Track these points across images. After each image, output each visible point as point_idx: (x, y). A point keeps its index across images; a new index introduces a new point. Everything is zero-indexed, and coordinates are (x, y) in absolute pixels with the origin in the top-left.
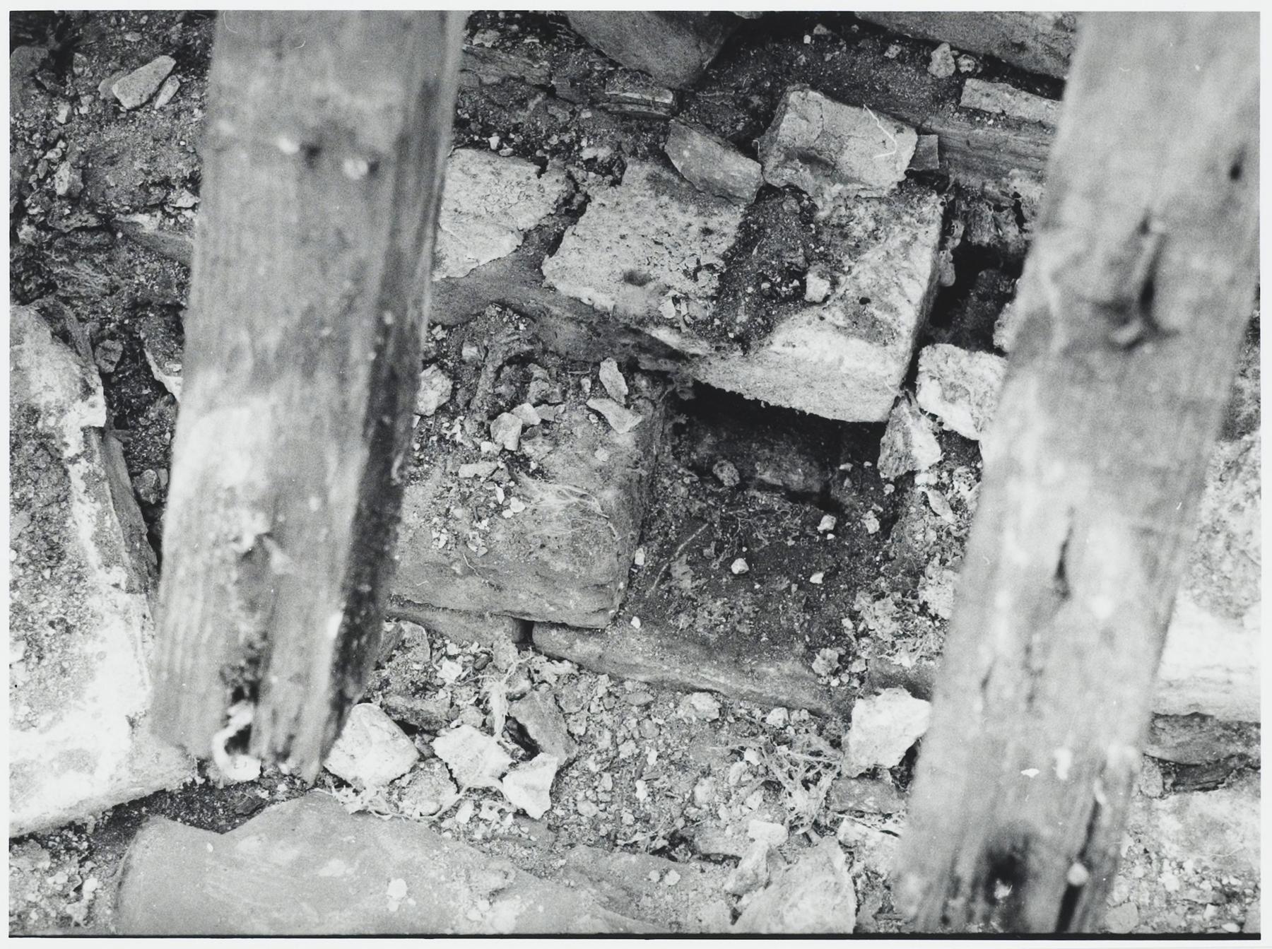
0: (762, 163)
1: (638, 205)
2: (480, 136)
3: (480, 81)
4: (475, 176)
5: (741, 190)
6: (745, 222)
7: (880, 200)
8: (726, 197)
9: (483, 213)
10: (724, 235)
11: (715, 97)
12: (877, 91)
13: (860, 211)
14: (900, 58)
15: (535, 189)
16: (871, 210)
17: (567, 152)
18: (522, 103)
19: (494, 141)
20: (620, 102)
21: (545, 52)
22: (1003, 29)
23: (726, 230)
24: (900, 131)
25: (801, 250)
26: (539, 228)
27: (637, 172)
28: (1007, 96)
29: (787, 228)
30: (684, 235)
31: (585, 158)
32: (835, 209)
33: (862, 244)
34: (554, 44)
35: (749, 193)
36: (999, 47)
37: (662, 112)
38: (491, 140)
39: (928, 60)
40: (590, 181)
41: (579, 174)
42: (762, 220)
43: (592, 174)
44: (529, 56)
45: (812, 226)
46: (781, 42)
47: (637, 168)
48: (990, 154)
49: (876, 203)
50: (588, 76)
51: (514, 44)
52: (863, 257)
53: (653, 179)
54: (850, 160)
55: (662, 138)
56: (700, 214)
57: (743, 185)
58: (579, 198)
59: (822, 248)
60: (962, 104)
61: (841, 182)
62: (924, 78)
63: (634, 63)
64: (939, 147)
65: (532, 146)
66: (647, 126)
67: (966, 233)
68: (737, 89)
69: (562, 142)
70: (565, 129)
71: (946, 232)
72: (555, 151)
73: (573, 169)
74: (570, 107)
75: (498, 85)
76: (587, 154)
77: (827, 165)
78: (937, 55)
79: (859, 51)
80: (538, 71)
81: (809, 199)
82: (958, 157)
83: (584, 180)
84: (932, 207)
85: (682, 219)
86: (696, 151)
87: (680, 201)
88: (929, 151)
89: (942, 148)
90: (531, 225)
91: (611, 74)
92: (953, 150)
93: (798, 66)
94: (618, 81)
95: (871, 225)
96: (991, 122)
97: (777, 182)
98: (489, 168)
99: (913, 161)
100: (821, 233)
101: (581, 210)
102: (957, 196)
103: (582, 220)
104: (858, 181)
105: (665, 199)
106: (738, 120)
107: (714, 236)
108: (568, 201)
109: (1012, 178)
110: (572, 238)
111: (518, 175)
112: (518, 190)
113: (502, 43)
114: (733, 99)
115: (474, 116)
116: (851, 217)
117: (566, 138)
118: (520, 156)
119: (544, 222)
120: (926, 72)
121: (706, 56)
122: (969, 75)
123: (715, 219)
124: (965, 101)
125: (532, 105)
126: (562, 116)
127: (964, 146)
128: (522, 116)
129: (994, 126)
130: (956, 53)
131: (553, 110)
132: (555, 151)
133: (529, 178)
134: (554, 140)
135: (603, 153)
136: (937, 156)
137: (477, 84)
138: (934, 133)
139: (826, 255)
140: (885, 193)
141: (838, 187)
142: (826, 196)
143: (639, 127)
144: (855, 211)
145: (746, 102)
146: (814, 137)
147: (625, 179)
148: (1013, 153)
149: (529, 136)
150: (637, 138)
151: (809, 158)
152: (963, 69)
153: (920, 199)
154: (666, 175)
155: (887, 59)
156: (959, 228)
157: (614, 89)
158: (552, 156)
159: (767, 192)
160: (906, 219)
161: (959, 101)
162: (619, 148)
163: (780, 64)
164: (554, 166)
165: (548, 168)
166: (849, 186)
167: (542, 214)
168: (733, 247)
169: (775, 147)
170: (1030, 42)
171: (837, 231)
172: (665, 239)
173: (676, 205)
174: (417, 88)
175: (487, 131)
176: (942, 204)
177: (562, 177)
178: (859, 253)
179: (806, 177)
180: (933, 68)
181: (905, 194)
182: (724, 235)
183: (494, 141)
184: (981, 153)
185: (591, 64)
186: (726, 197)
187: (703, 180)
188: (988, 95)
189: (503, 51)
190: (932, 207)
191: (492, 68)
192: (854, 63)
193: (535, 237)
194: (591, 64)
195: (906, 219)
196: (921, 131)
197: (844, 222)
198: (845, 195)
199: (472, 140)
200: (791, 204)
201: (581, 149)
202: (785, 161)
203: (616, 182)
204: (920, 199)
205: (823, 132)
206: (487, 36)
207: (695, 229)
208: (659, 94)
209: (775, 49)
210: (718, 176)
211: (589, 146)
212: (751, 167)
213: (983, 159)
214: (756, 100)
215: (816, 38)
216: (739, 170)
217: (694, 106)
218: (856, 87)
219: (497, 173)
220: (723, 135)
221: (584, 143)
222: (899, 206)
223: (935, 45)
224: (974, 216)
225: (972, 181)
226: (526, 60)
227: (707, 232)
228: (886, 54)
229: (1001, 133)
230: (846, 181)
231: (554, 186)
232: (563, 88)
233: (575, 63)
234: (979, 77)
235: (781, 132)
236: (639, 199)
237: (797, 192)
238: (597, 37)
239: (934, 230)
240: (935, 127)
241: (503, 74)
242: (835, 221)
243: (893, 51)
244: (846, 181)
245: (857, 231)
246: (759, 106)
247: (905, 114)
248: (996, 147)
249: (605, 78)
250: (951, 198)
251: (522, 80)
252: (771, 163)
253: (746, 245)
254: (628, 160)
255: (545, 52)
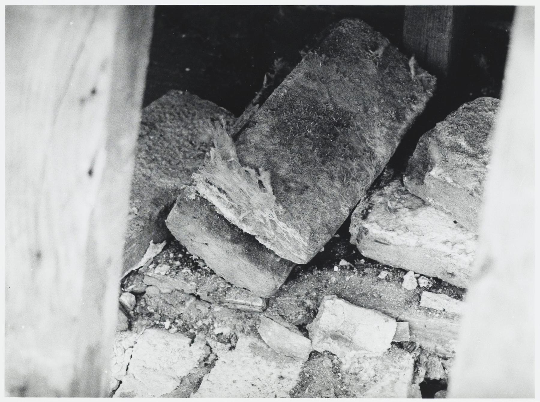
0: (311, 340)
1: (244, 362)
2: (160, 321)
3: (160, 291)
4: (155, 345)
5: (300, 354)
6: (303, 372)
7: (377, 358)
8: (292, 358)
9: (158, 368)
10: (291, 379)
11: (285, 300)
12: (374, 297)
13: (366, 365)
14: (387, 279)
15: (188, 353)
16: (373, 364)
17: (206, 329)
18: (182, 303)
19: (167, 324)
20: (234, 304)
21: (193, 277)
22: (442, 265)
23: (292, 377)
24: (387, 321)
25: (333, 389)
26: (190, 375)
27: (244, 342)
28: (446, 301)
29: (325, 377)
30: (268, 380)
31: (216, 333)
32: (352, 365)
33: (367, 385)
34: (199, 272)
35: (305, 356)
36: (440, 273)
37: (257, 309)
38: (165, 323)
39: (402, 280)
40: (218, 347)
41: (212, 343)
42: (311, 371)
43: (219, 344)
44: (185, 279)
45: (339, 374)
46: (322, 270)
47: (244, 339)
48: (437, 332)
49: (375, 360)
50: (216, 291)
51: (177, 273)
52: (368, 392)
53: (253, 347)
54: (358, 338)
55: (257, 323)
56: (278, 367)
57: (301, 351)
58: (212, 357)
59: (345, 388)
60: (421, 305)
61: (355, 349)
62: (400, 290)
63: (241, 285)
64: (409, 328)
65: (188, 326)
66: (250, 316)
67: (427, 373)
68: (298, 296)
69: (204, 324)
70: (206, 317)
71: (416, 373)
72: (201, 329)
73: (209, 341)
74: (208, 305)
75: (169, 293)
76: (217, 331)
77: (347, 340)
78: (406, 277)
79: (364, 275)
80: (190, 287)
81: (338, 359)
82: (421, 333)
83: (215, 347)
84: (408, 359)
85: (268, 371)
86: (275, 332)
87: (267, 359)
88: (404, 331)
89: (410, 328)
90: (185, 374)
91: (228, 289)
92: (417, 329)
93: (331, 283)
94: (233, 293)
95: (372, 373)
96: (437, 315)
97: (320, 350)
98: (163, 341)
99: (395, 336)
100: (345, 378)
101: (212, 365)
102: (421, 352)
103: (213, 370)
104: (365, 349)
105: (258, 358)
106: (299, 313)
107: (285, 380)
108: (206, 359)
109: (451, 344)
110: (207, 382)
111: (178, 345)
112: (178, 354)
113: (170, 273)
114: (296, 302)
115: (156, 311)
116: (361, 369)
117: (206, 322)
118: (181, 333)
119: (192, 372)
120: (401, 287)
121: (278, 283)
122: (425, 289)
123: (286, 370)
124: (423, 303)
125: (188, 304)
126: (204, 309)
127: (423, 327)
128: (182, 310)
129: (439, 317)
130: (418, 275)
131: (199, 307)
132: (201, 329)
133: (184, 347)
134: (200, 323)
135: (227, 331)
136: (408, 333)
137: (158, 293)
138: (406, 321)
139: (347, 392)
140: (380, 355)
141: (354, 352)
142: (346, 357)
143: (246, 316)
144: (363, 365)
145: (303, 303)
146: (340, 324)
147: (238, 346)
148: (450, 331)
149: (186, 321)
150: (245, 323)
151: (336, 337)
152: (421, 285)
153: (400, 357)
154: (260, 344)
155: (380, 280)
156: (422, 371)
157: (231, 297)
158: (199, 332)
159: (313, 354)
160: (392, 369)
161: (419, 304)
162: (235, 328)
163: (321, 282)
164: (199, 338)
165: (196, 340)
166: (359, 352)
167: (191, 368)
168: (296, 387)
169: (318, 330)
170: (456, 272)
171: (353, 377)
172: (257, 382)
173: (264, 361)
174: (83, 351)
175: (163, 318)
176: (413, 358)
177: (203, 345)
178: (366, 390)
179: (334, 347)
180: (405, 284)
181: (391, 354)
182: (291, 379)
183: (167, 324)
184: (433, 331)
185: (218, 284)
186: (292, 358)
187: (279, 348)
188: (435, 301)
189: (171, 276)
190: (408, 359)
191: (165, 285)
192: (362, 282)
193: (187, 381)
194: (218, 284)
195: (392, 369)
196: (398, 320)
197: (357, 371)
198: (357, 356)
199: (155, 324)
200: (327, 363)
201: (214, 328)
202: (323, 339)
203: (232, 348)
204: (400, 357)
205: (345, 321)
206: (162, 268)
207: (275, 376)
208: (255, 300)
209: (319, 274)
210: (287, 346)
211: (218, 327)
212: (305, 341)
213: (435, 334)
214: (309, 302)
215: (342, 268)
216: (299, 344)
217: (275, 305)
218: (363, 295)
219: (167, 344)
220: (290, 322)
221: (216, 325)
222: (388, 361)
223: (406, 272)
224: (431, 364)
225: (429, 346)
226: (183, 281)
227: (281, 377)
228: (379, 276)
229: (445, 322)
230: (358, 349)
231: (198, 351)
232: (204, 296)
233: (209, 283)
234: (430, 290)
235: (321, 322)
236: (244, 358)
237: (331, 355)
238: (220, 271)
239: (410, 372)
240: (407, 318)
241: (172, 288)
242: (352, 371)
243: (383, 274)
244: (358, 349)
245: (364, 377)
246: (310, 305)
247: (390, 311)
248: (440, 329)
249: (225, 292)
250: (418, 354)
251: (183, 291)
252: (316, 340)
253: (302, 386)
254: (239, 335)
255: (193, 277)
